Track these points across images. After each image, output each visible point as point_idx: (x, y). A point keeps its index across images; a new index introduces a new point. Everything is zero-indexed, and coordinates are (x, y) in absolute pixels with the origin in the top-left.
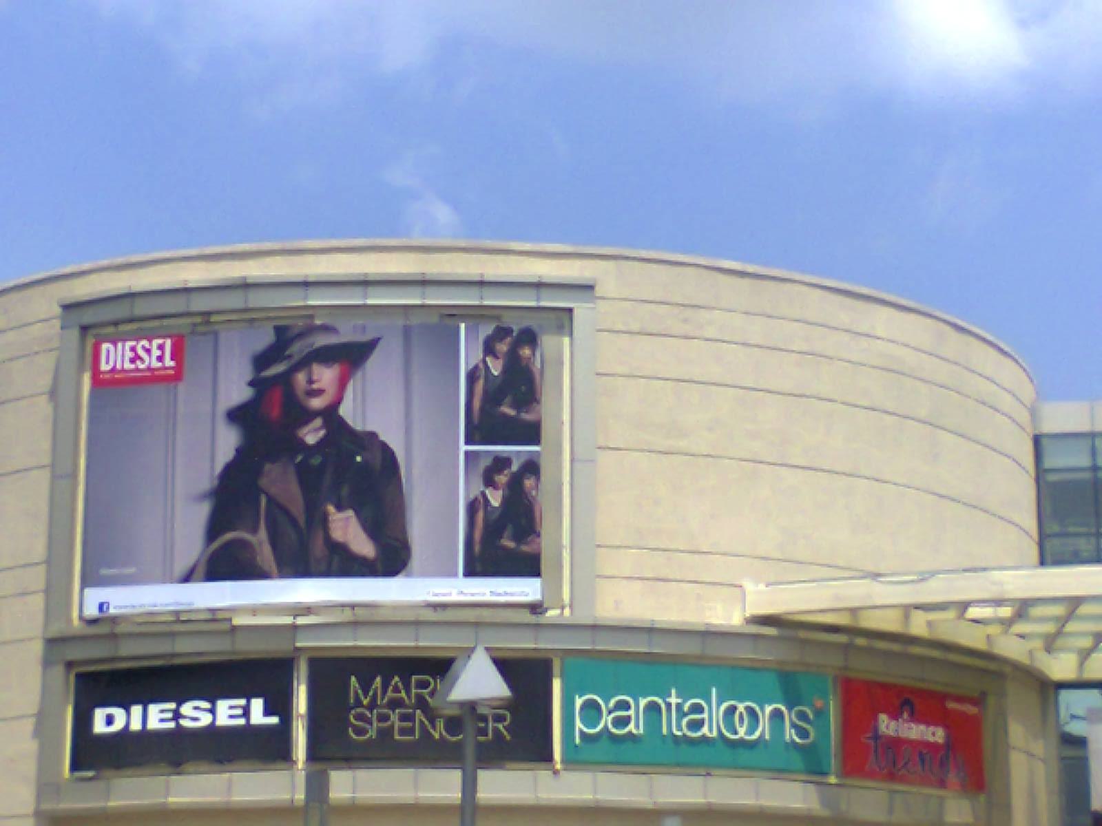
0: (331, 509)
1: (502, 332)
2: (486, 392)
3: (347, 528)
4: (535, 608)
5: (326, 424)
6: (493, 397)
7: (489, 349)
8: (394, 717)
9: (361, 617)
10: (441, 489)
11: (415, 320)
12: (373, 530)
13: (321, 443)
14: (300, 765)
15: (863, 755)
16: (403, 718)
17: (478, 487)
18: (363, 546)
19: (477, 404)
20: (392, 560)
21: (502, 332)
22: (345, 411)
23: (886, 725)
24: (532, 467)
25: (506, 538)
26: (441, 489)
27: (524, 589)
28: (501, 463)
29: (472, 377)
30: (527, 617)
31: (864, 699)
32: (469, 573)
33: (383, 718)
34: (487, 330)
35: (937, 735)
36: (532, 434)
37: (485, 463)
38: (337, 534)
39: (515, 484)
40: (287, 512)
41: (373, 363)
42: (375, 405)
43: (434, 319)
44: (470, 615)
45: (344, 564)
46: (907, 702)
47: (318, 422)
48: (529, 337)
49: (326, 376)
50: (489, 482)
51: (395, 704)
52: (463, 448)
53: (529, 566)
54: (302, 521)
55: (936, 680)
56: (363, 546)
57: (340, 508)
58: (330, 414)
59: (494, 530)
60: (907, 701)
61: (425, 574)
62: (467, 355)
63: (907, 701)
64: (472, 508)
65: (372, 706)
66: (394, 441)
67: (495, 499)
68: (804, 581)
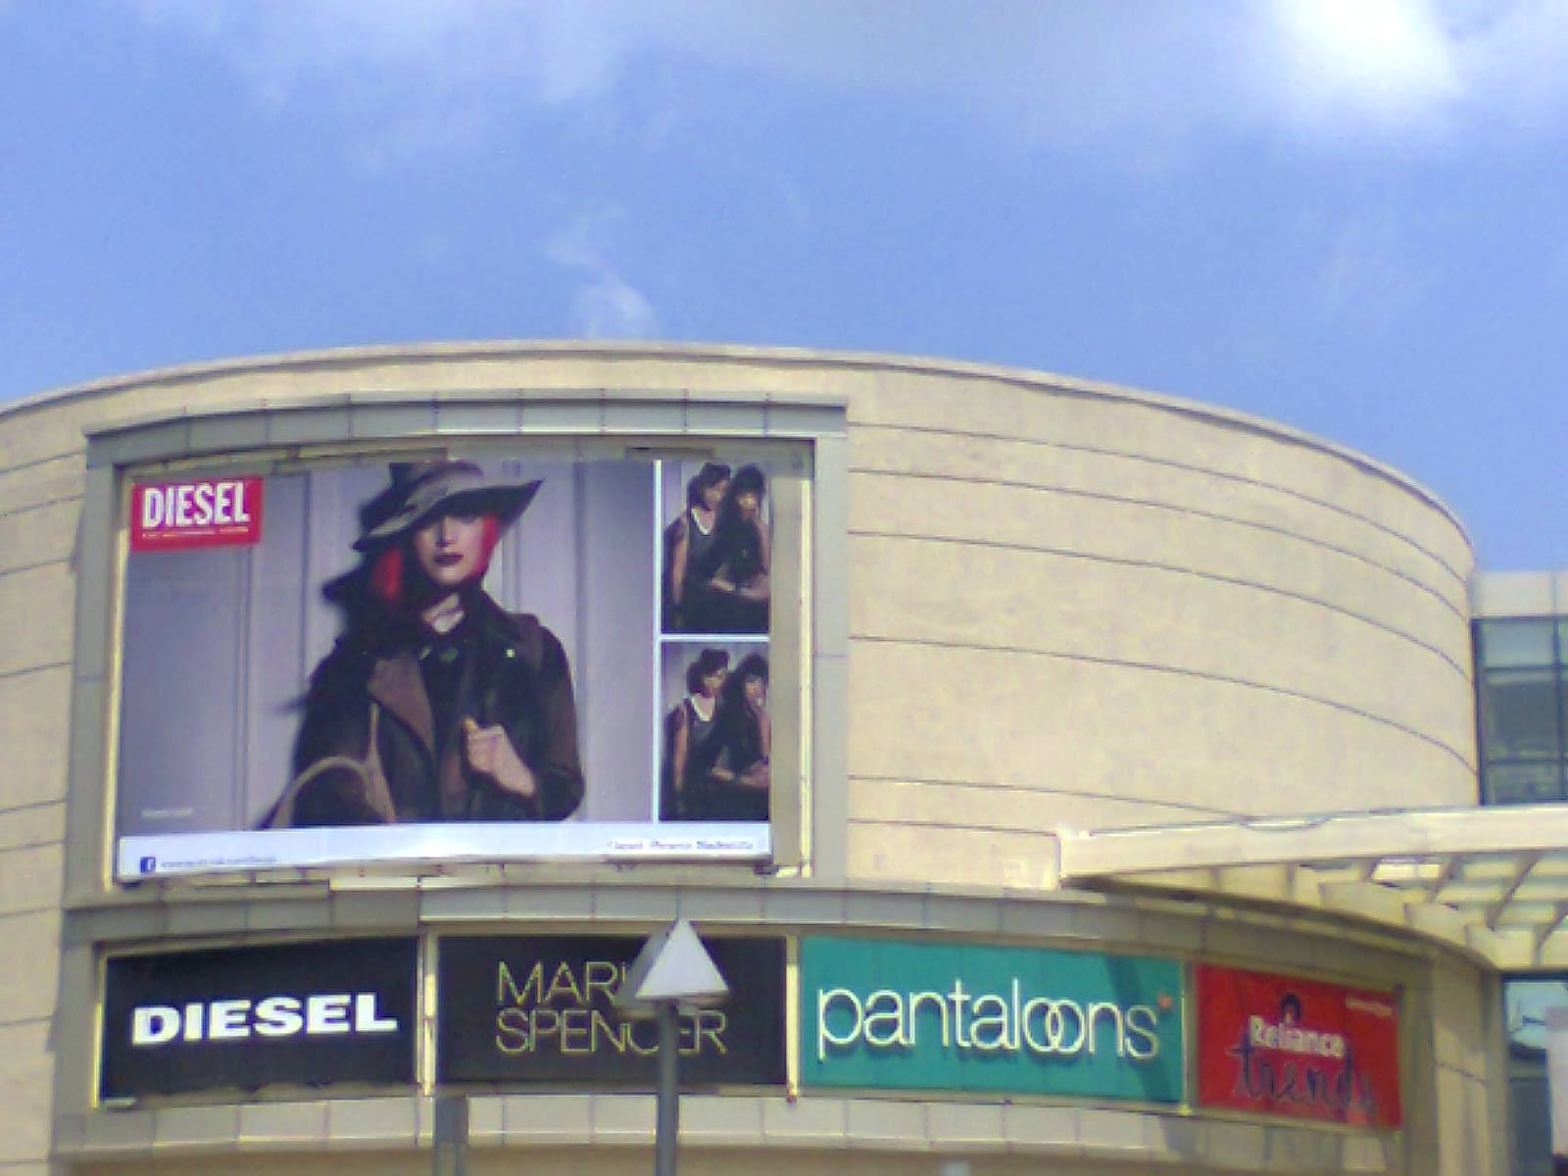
0: (471, 724)
1: (714, 473)
2: (691, 558)
3: (494, 752)
4: (762, 866)
5: (464, 604)
6: (702, 565)
7: (696, 497)
8: (561, 1021)
9: (514, 878)
10: (627, 697)
11: (590, 456)
12: (531, 754)
13: (457, 631)
14: (427, 1089)
15: (1228, 1074)
16: (574, 1022)
17: (680, 693)
18: (517, 777)
19: (678, 575)
20: (558, 797)
21: (714, 473)
22: (491, 585)
23: (1261, 1032)
24: (757, 665)
25: (721, 765)
26: (627, 697)
27: (745, 839)
28: (713, 659)
29: (671, 537)
30: (750, 878)
31: (1229, 995)
32: (668, 815)
33: (545, 1022)
34: (693, 470)
35: (1333, 1046)
36: (756, 617)
37: (690, 658)
38: (480, 761)
39: (733, 689)
40: (408, 729)
41: (531, 517)
42: (534, 577)
43: (618, 455)
44: (668, 876)
45: (489, 803)
46: (1290, 1000)
47: (453, 601)
48: (753, 480)
49: (463, 535)
50: (696, 686)
51: (562, 1002)
52: (659, 637)
53: (753, 806)
54: (429, 741)
55: (1332, 969)
56: (517, 777)
57: (483, 723)
58: (470, 590)
59: (703, 754)
60: (1291, 999)
61: (605, 817)
62: (665, 505)
63: (1291, 999)
64: (671, 723)
65: (529, 1006)
66: (561, 627)
67: (705, 710)
68: (1144, 827)
